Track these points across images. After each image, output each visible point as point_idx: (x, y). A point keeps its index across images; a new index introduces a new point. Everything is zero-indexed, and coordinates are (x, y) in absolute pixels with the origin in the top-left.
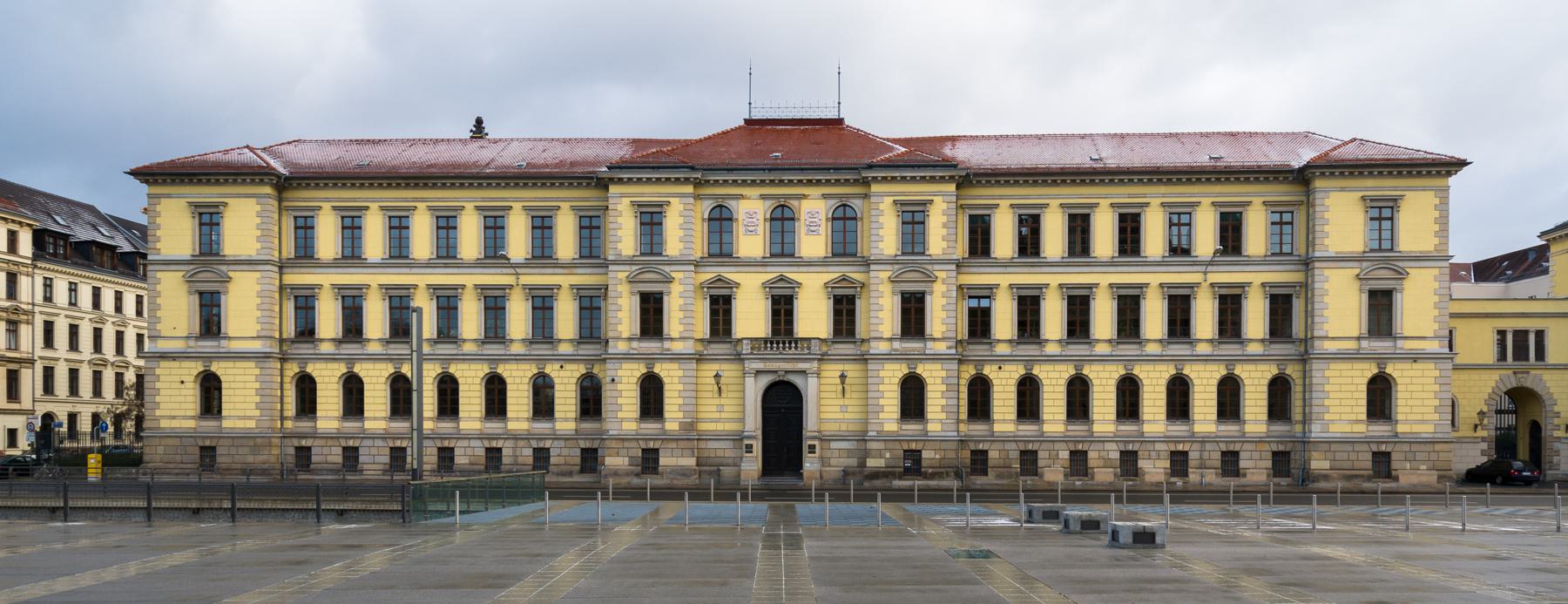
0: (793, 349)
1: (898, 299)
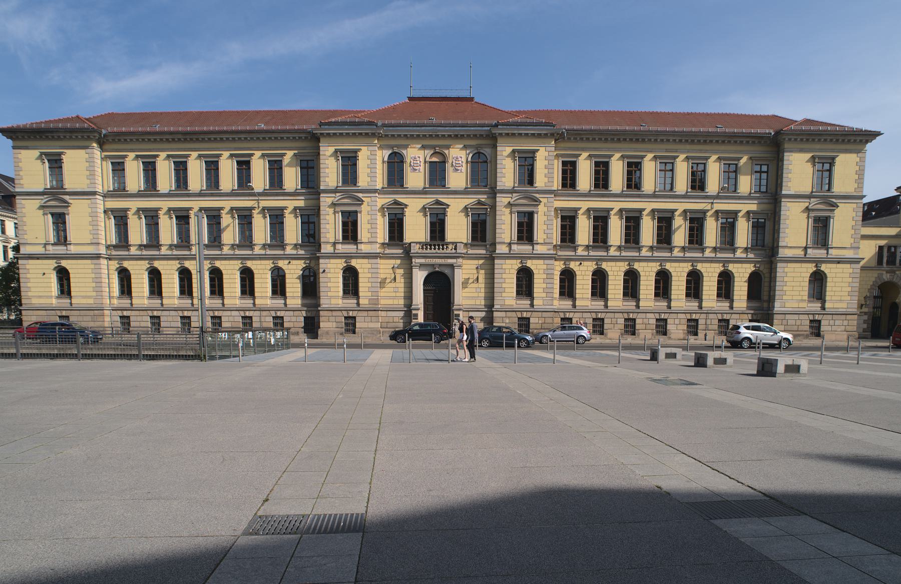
0: (433, 249)
1: (515, 217)
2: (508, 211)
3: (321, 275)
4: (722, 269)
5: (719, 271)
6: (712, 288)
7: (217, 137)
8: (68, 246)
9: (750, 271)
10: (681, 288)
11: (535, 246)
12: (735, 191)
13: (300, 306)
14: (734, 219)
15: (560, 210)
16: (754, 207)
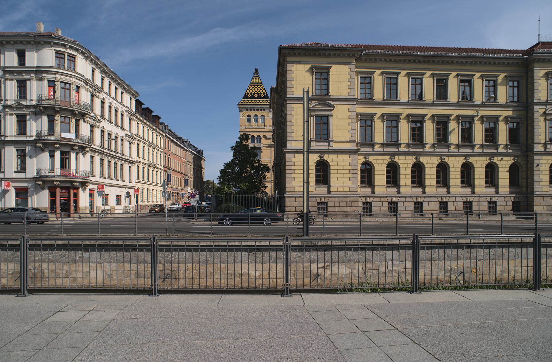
2: (543, 119)
3: (535, 169)
4: (390, 160)
5: (437, 163)
6: (407, 176)
7: (463, 60)
8: (331, 143)
9: (510, 163)
10: (432, 177)
11: (331, 143)
12: (396, 99)
13: (508, 193)
14: (397, 121)
15: (361, 115)
16: (510, 113)
